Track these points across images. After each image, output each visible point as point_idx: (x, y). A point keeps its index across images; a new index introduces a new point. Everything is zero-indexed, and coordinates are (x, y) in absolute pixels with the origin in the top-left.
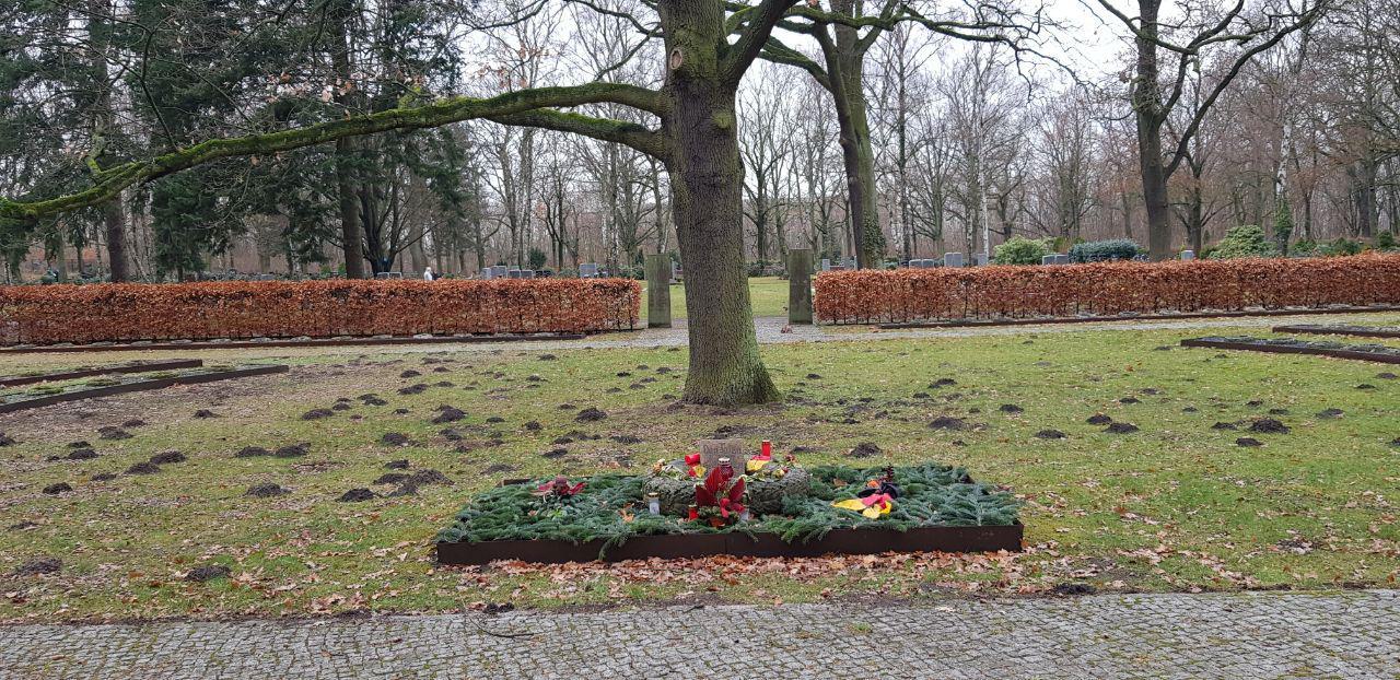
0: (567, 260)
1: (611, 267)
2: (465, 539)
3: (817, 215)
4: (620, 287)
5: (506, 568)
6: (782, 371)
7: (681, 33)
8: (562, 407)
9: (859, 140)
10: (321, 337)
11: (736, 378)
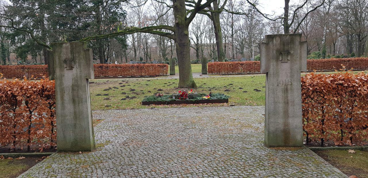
0: (148, 59)
1: (160, 62)
2: (146, 101)
3: (212, 48)
4: (164, 66)
6: (199, 83)
7: (178, 16)
8: (154, 89)
9: (219, 32)
10: (97, 77)
11: (189, 83)
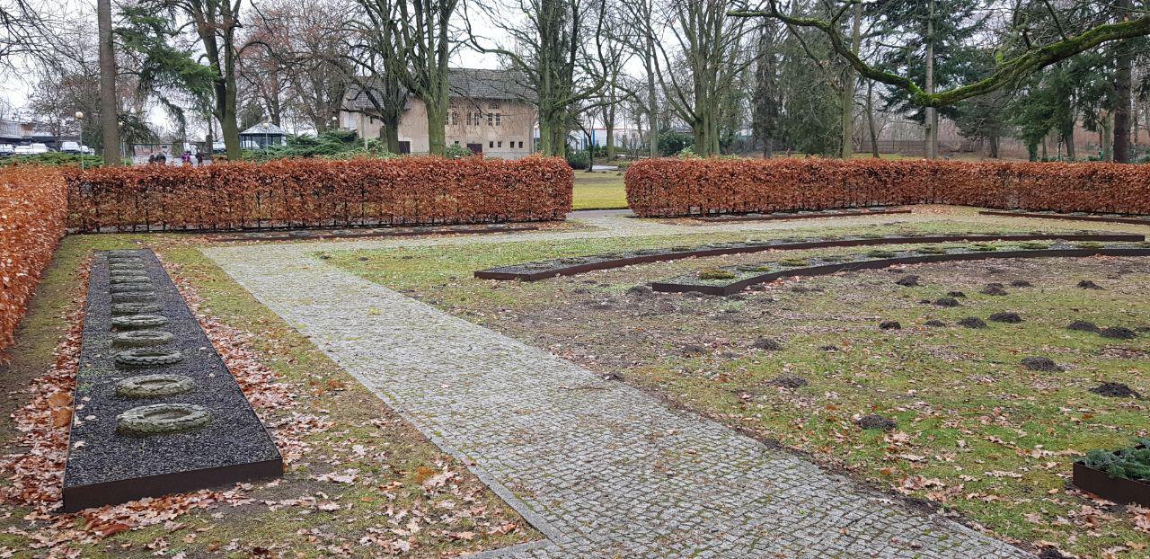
5: (1139, 517)
